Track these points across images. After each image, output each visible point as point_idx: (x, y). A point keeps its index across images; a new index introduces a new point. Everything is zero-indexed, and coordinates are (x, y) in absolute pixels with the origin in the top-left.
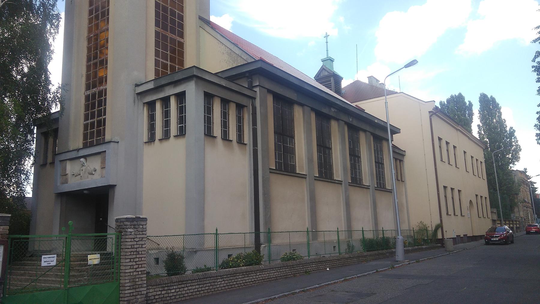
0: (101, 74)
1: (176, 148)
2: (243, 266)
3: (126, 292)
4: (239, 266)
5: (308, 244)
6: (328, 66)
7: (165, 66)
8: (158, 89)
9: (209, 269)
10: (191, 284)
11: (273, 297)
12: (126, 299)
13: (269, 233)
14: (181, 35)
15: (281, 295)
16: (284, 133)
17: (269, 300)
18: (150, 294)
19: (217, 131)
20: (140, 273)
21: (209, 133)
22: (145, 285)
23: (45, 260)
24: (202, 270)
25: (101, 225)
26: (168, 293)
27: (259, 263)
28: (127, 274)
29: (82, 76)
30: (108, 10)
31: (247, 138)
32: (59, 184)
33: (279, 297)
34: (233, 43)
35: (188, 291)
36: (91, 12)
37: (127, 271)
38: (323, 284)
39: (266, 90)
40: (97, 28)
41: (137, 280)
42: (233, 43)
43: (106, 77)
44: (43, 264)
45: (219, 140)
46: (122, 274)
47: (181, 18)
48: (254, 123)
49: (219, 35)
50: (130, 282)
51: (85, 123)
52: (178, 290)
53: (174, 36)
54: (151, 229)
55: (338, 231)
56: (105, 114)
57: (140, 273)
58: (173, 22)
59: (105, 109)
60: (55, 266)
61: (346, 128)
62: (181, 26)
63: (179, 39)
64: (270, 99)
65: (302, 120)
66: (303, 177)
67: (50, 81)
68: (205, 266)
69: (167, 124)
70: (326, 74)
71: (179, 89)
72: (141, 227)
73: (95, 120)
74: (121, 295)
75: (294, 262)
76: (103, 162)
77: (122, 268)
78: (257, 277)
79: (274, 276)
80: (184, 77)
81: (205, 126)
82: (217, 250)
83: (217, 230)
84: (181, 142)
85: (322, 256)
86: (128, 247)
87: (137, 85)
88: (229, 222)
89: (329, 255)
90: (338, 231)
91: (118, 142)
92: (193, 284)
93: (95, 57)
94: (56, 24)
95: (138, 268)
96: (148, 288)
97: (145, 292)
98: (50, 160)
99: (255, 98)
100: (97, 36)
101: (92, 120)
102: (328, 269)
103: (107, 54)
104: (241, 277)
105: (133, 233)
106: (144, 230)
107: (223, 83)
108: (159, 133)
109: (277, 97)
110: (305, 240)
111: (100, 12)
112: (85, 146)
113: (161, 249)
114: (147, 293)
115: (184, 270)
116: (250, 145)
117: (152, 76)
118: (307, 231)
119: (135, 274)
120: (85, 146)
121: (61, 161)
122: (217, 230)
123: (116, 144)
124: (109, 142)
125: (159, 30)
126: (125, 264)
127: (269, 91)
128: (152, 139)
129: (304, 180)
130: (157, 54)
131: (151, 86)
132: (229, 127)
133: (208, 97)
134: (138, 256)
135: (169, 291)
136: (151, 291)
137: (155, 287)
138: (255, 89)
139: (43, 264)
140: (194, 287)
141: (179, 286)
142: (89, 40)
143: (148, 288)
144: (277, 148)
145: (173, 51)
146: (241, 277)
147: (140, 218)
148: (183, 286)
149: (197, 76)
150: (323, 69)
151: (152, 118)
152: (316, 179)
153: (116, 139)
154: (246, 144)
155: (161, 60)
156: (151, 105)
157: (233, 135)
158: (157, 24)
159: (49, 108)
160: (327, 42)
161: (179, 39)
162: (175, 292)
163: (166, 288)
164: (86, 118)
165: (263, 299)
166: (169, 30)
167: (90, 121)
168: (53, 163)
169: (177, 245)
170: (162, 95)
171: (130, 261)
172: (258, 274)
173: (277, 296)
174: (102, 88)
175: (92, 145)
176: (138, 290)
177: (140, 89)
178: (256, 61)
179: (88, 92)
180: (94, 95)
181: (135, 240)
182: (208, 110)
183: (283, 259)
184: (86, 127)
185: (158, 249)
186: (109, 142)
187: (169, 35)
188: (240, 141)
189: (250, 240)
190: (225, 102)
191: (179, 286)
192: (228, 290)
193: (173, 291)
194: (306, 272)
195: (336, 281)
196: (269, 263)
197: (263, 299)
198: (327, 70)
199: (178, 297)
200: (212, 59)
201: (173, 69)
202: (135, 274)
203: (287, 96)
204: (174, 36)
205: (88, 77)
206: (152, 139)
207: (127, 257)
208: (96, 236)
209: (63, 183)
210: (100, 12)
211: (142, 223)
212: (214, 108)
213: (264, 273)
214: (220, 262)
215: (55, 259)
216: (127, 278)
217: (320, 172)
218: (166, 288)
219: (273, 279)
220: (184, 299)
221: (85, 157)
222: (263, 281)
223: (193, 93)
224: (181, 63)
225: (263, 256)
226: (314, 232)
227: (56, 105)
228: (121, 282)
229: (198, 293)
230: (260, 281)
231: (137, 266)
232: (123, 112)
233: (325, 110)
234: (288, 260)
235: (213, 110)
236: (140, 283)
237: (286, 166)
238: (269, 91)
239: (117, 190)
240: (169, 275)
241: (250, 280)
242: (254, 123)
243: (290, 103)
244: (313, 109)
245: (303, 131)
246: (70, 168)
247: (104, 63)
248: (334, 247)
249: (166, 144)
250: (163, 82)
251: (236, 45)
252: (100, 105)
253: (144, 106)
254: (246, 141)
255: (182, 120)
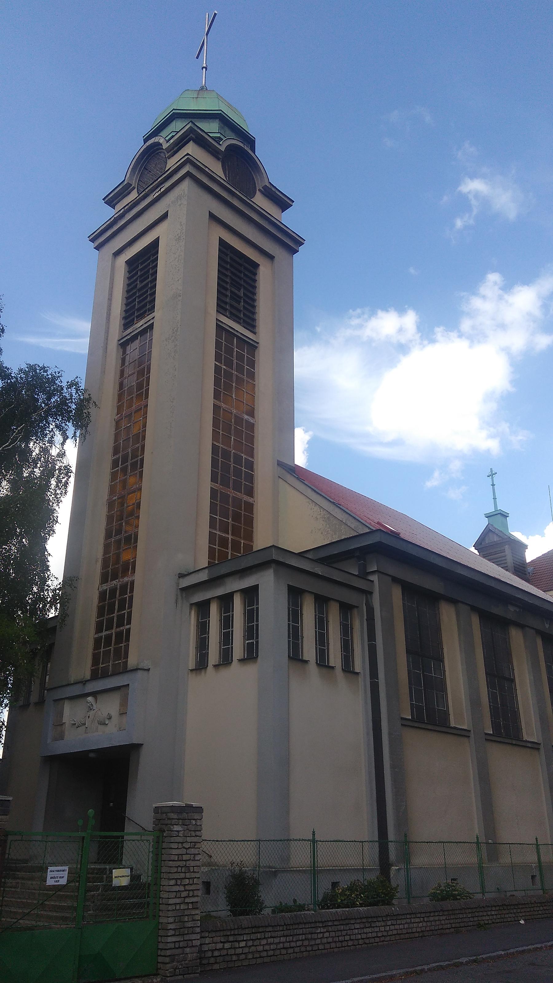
0: (125, 557)
1: (241, 680)
2: (361, 905)
3: (170, 939)
4: (354, 905)
5: (481, 869)
6: (498, 526)
7: (223, 542)
8: (215, 581)
9: (301, 908)
10: (273, 934)
11: (419, 968)
12: (168, 953)
13: (406, 844)
14: (250, 492)
15: (434, 965)
16: (425, 652)
17: (412, 973)
18: (205, 948)
19: (309, 651)
20: (190, 906)
21: (295, 656)
22: (198, 930)
23: (55, 874)
24: (288, 909)
25: (113, 815)
26: (235, 948)
27: (389, 903)
28: (170, 908)
29: (97, 561)
30: (142, 460)
31: (360, 663)
32: (49, 741)
33: (429, 970)
34: (333, 503)
35: (267, 947)
36: (115, 464)
37: (171, 901)
38: (512, 951)
39: (390, 579)
40: (124, 487)
41: (186, 919)
42: (333, 503)
43: (134, 562)
44: (50, 882)
45: (313, 667)
46: (162, 907)
47: (250, 466)
48: (372, 636)
49: (309, 490)
50: (175, 922)
51: (96, 636)
52: (250, 943)
53: (239, 495)
54: (210, 827)
55: (537, 845)
56: (129, 623)
57: (190, 906)
58: (238, 473)
59: (130, 614)
60: (64, 886)
61: (539, 642)
62: (251, 478)
63: (246, 498)
64: (397, 593)
65: (455, 628)
66: (463, 734)
67: (48, 566)
68: (295, 901)
69: (227, 638)
70: (496, 539)
71: (248, 582)
72: (194, 822)
73: (113, 631)
74: (161, 946)
75: (456, 902)
76: (124, 703)
77: (164, 895)
78: (388, 928)
79: (419, 930)
80: (257, 562)
81: (289, 642)
82: (314, 872)
83: (314, 834)
84: (251, 669)
85: (508, 894)
86: (173, 857)
87: (182, 576)
88: (332, 820)
89: (523, 893)
90: (537, 845)
91: (148, 670)
92: (276, 934)
93: (119, 532)
94: (63, 480)
95: (188, 896)
96: (203, 934)
97: (198, 943)
98: (34, 698)
99: (371, 593)
100: (122, 498)
101: (107, 632)
102: (522, 922)
103: (137, 527)
104: (357, 926)
105: (181, 835)
106: (198, 829)
107: (319, 570)
108: (213, 656)
109: (409, 590)
110: (474, 860)
111: (129, 463)
112: (95, 676)
113: (216, 864)
114: (201, 945)
115: (259, 906)
116: (365, 675)
117: (204, 562)
118: (478, 843)
119: (182, 907)
120: (95, 676)
121: (55, 701)
122: (314, 834)
123: (145, 673)
124: (136, 670)
125: (217, 486)
126: (167, 888)
127: (395, 580)
128: (201, 665)
129: (466, 739)
130: (212, 523)
131: (203, 576)
132: (328, 644)
133: (295, 594)
134: (188, 875)
135: (237, 945)
136: (207, 941)
137: (213, 934)
138: (371, 578)
139: (50, 882)
140: (277, 940)
141: (253, 937)
142: (111, 504)
143: (203, 934)
144: (413, 679)
145: (237, 517)
146: (357, 926)
147: (191, 806)
148: (259, 936)
149: (275, 560)
150: (488, 531)
151: (203, 628)
152: (489, 738)
153: (145, 664)
154: (357, 674)
155: (218, 533)
156: (203, 608)
157: (335, 657)
158: (214, 479)
159: (44, 610)
160: (493, 485)
161: (246, 498)
162: (246, 946)
163: (231, 938)
164: (99, 629)
165: (402, 971)
166: (231, 485)
167: (104, 633)
168: (41, 702)
169: (246, 857)
170: (220, 591)
171: (176, 885)
172: (389, 923)
173: (426, 967)
174: (126, 579)
175: (105, 675)
176: (187, 937)
177: (186, 582)
178: (372, 532)
179: (105, 587)
180: (113, 591)
181: (184, 845)
182: (295, 615)
183: (434, 897)
184: (97, 642)
185: (209, 864)
186: (136, 670)
187: (232, 493)
188: (348, 667)
189: (370, 856)
190: (321, 601)
191: (253, 937)
192: (336, 950)
193: (243, 944)
194: (479, 926)
195: (539, 946)
196: (409, 903)
197: (402, 971)
198: (497, 532)
199: (250, 956)
200: (297, 528)
201: (236, 546)
202: (182, 907)
203: (427, 587)
204: (239, 495)
205: (105, 563)
206: (201, 665)
207: (171, 876)
208: (101, 837)
209: (55, 739)
210: (129, 463)
211: (196, 816)
212: (304, 612)
213: (399, 922)
214: (320, 899)
215: (49, 875)
216: (170, 914)
217: (495, 726)
218: (231, 938)
219: (417, 935)
220: (259, 961)
221: (94, 694)
222: (398, 937)
223: (271, 589)
224: (249, 536)
225: (396, 888)
226: (490, 845)
227: (56, 608)
228: (161, 920)
229: (283, 952)
230: (393, 938)
231: (184, 894)
232: (159, 620)
233: (497, 610)
234: (444, 899)
235: (302, 615)
236: (190, 924)
237: (429, 715)
238: (395, 580)
239: (144, 752)
240: (234, 913)
241: (374, 935)
242: (372, 636)
243: (434, 598)
244: (474, 609)
245: (458, 648)
246: (70, 713)
247: (131, 540)
248: (533, 877)
249: (226, 673)
250: (224, 570)
251: (337, 505)
252: (122, 607)
253: (191, 609)
254: (358, 668)
255: (251, 632)
